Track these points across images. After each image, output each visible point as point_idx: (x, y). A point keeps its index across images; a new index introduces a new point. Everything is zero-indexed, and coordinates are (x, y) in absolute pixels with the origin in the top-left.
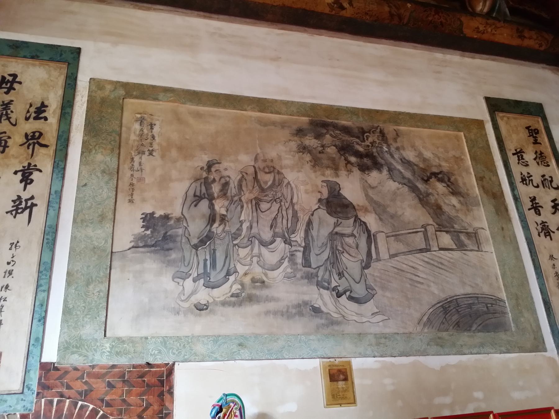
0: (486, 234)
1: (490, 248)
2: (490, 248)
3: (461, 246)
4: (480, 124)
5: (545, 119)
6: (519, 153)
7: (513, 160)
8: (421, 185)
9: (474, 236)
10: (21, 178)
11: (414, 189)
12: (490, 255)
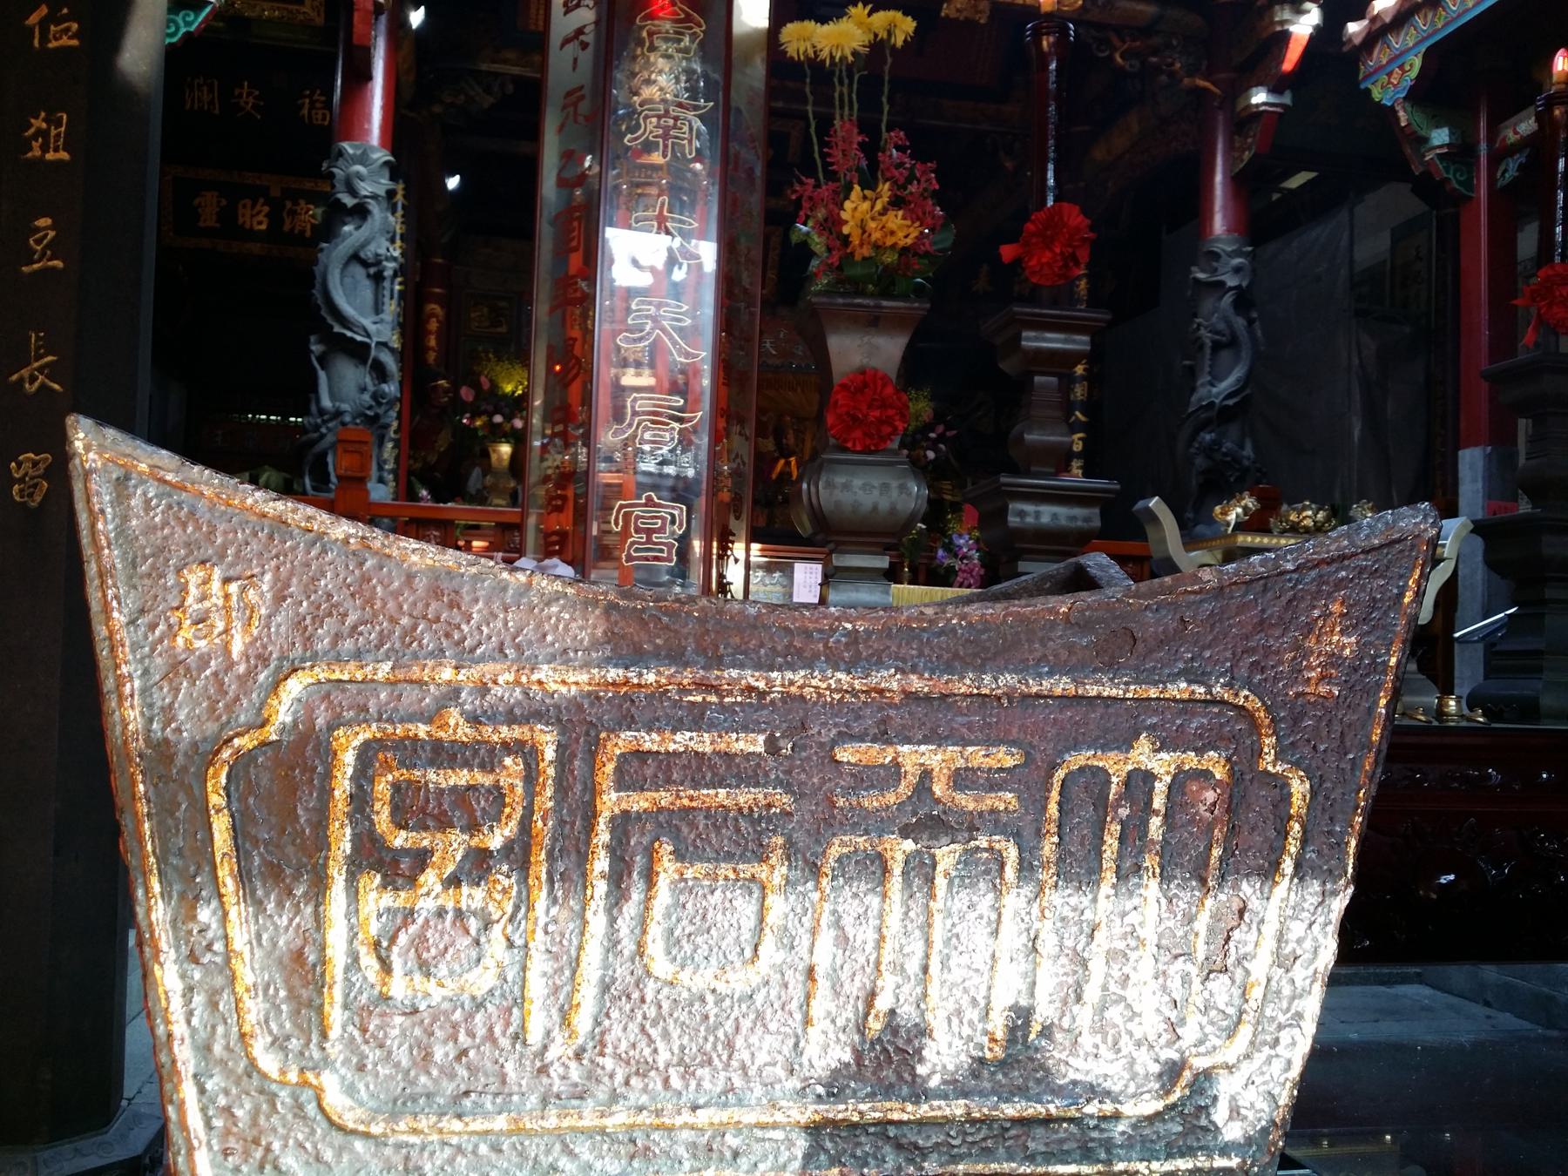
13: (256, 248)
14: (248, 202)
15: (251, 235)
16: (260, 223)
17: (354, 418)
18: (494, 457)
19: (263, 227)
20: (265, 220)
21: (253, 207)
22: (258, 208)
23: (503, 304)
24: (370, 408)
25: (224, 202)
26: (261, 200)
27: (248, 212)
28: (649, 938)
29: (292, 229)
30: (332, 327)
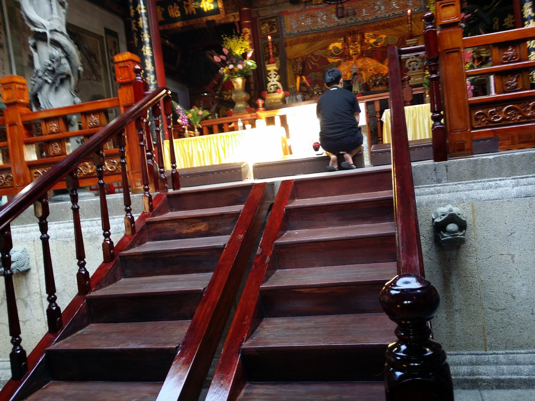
0: (103, 77)
1: (103, 82)
2: (103, 82)
3: (97, 80)
4: (102, 37)
5: (118, 40)
6: (111, 51)
7: (109, 52)
8: (88, 57)
9: (100, 77)
10: (250, 126)
11: (87, 58)
12: (103, 84)
13: (179, 24)
14: (171, 6)
15: (175, 20)
16: (177, 14)
17: (44, 73)
18: (235, 85)
19: (179, 15)
20: (179, 12)
21: (173, 8)
22: (175, 7)
23: (274, 20)
24: (50, 65)
25: (163, 9)
26: (175, 4)
27: (172, 10)
28: (303, 330)
29: (189, 13)
30: (30, 28)
